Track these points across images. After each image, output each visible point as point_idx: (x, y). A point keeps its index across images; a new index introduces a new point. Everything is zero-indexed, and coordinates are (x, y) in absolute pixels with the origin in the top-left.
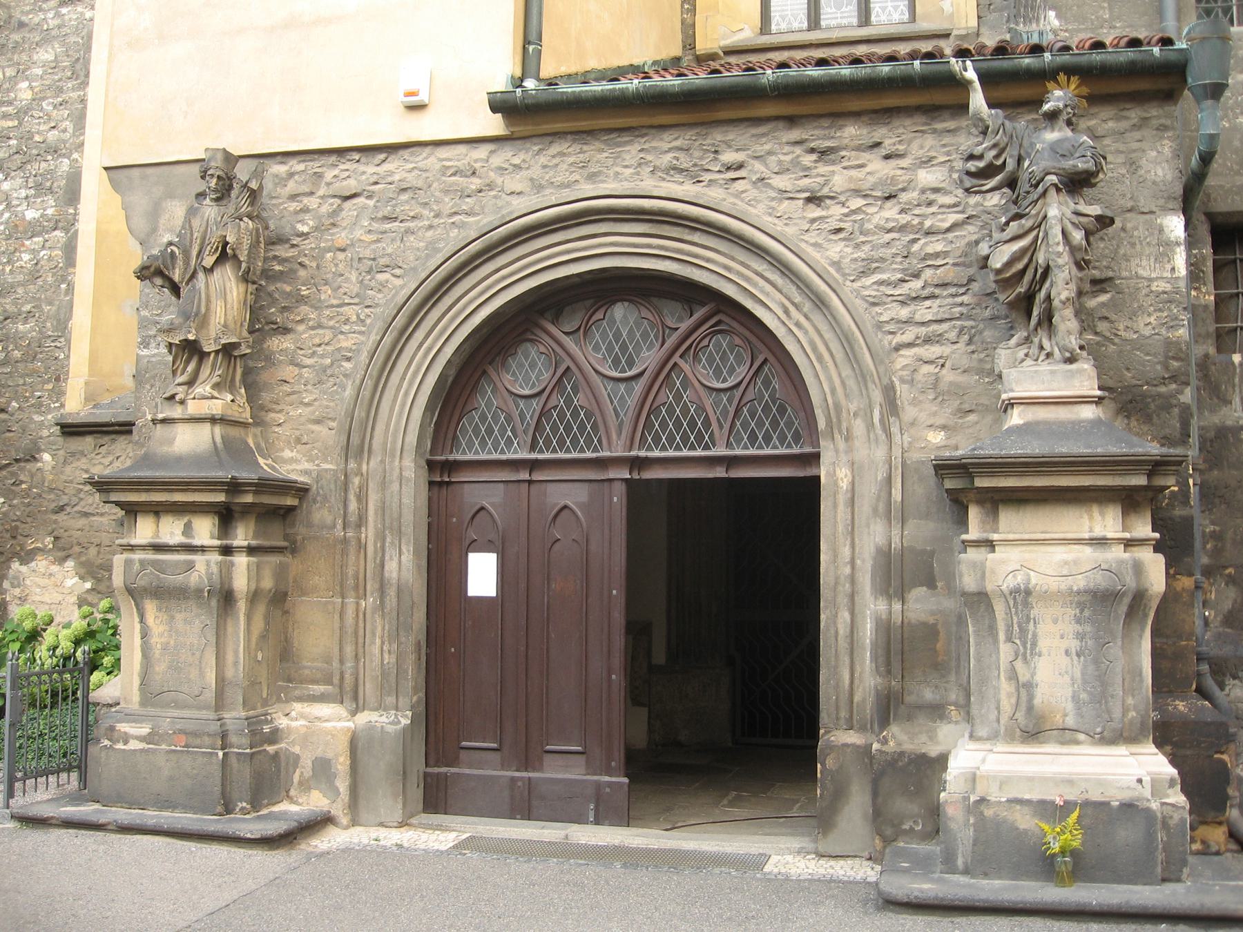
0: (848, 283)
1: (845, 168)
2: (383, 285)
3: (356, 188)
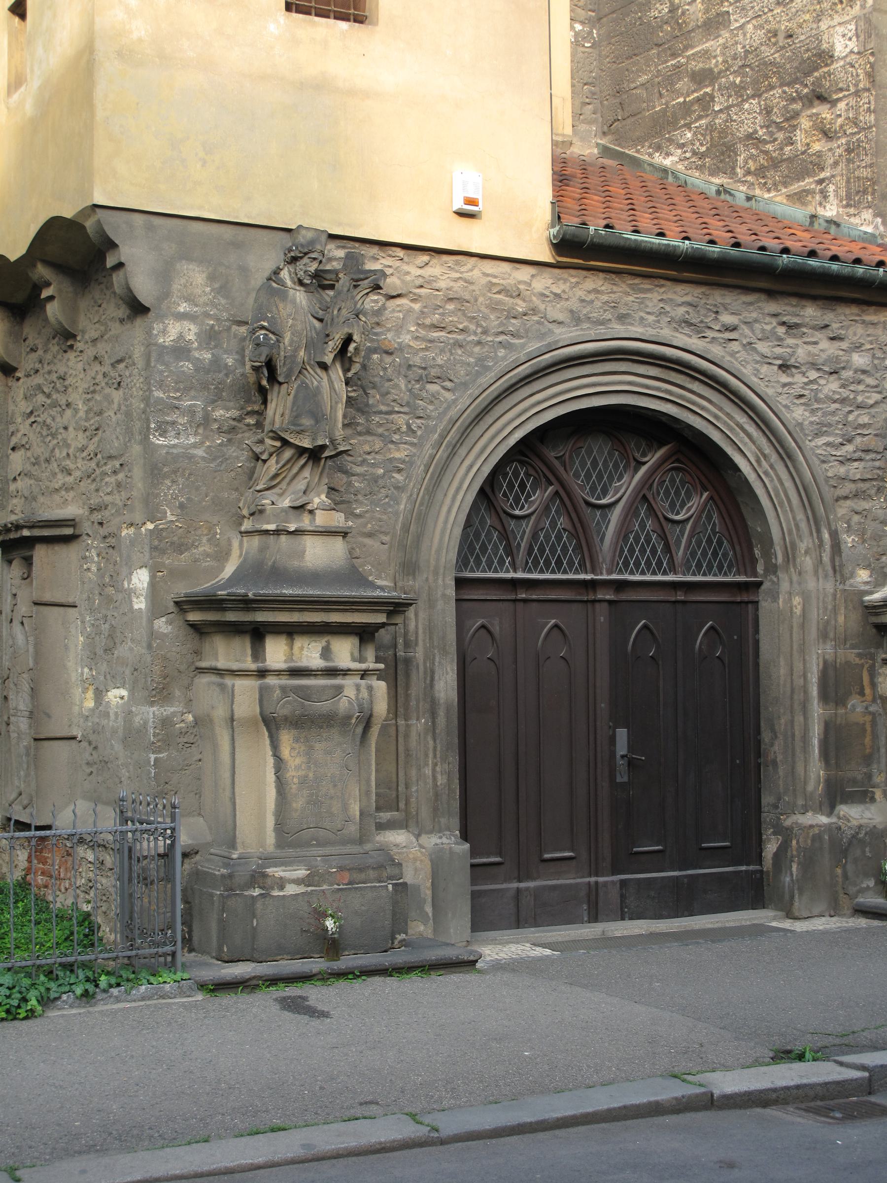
0: (807, 442)
1: (805, 343)
2: (435, 396)
3: (402, 289)
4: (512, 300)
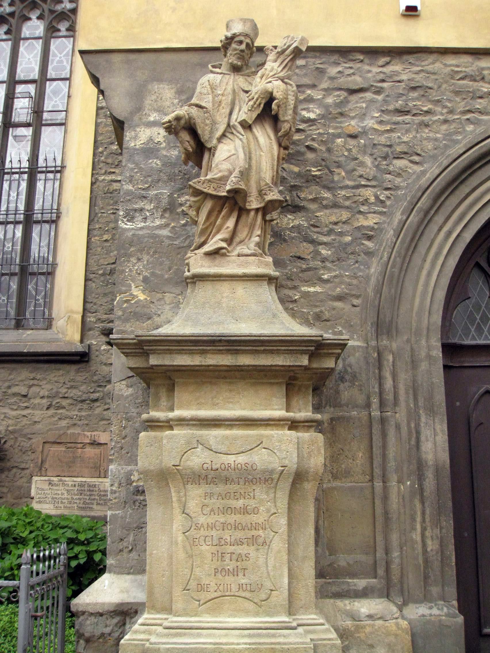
4: (476, 84)
